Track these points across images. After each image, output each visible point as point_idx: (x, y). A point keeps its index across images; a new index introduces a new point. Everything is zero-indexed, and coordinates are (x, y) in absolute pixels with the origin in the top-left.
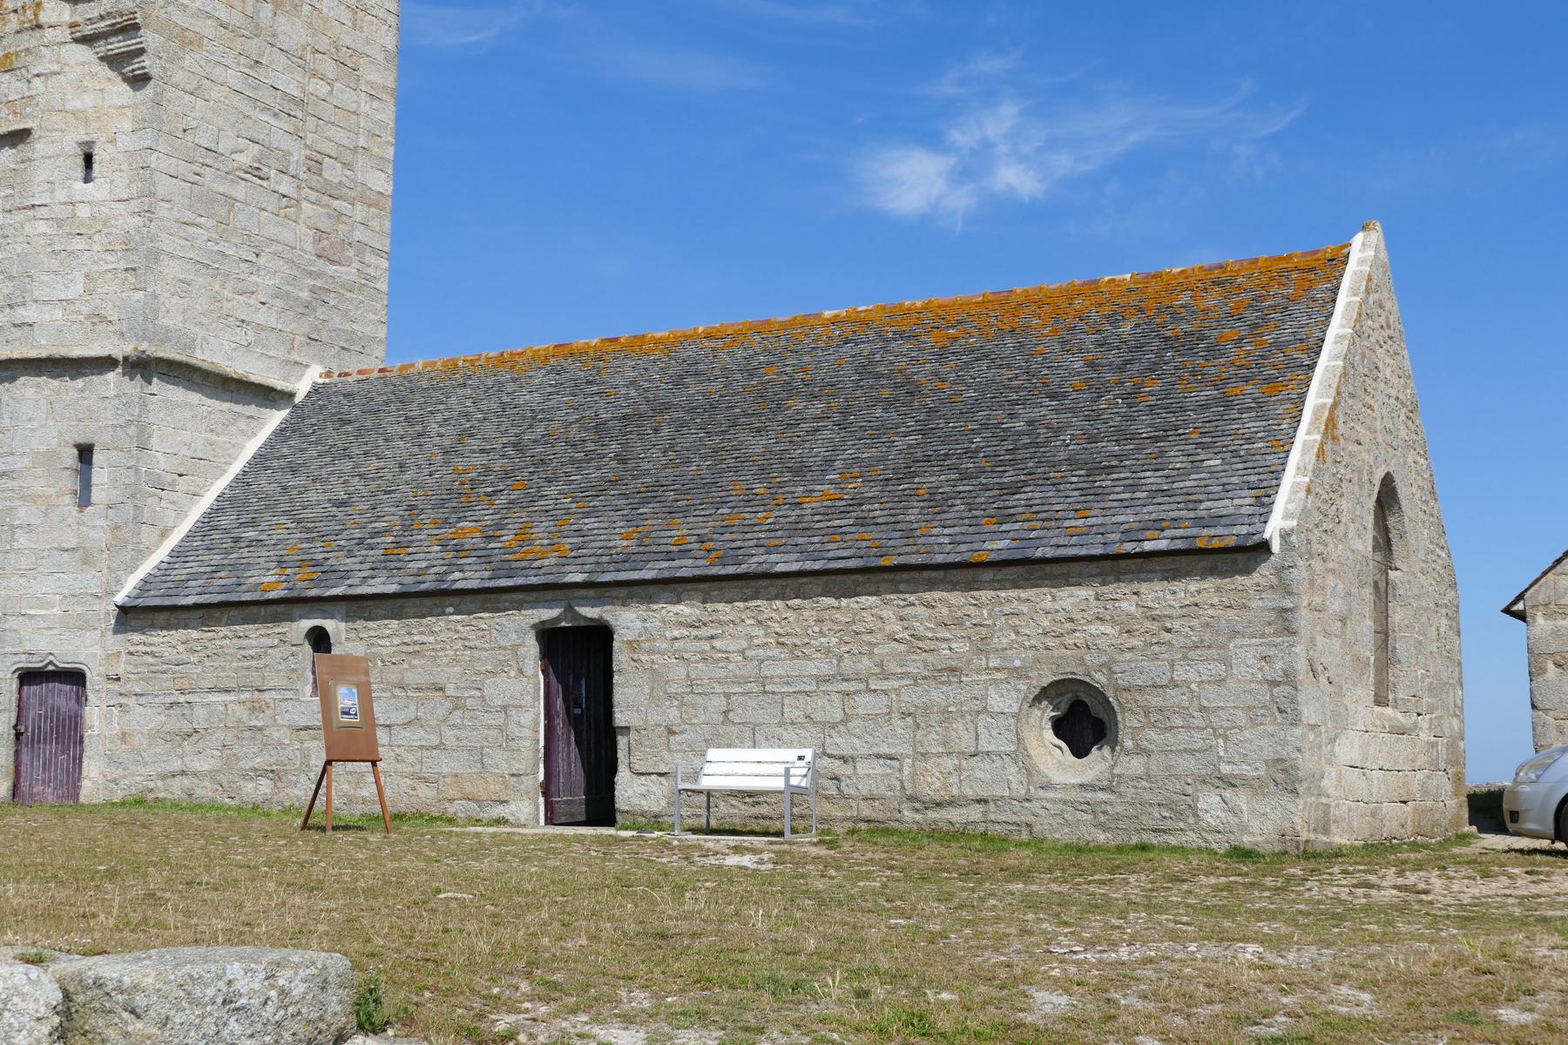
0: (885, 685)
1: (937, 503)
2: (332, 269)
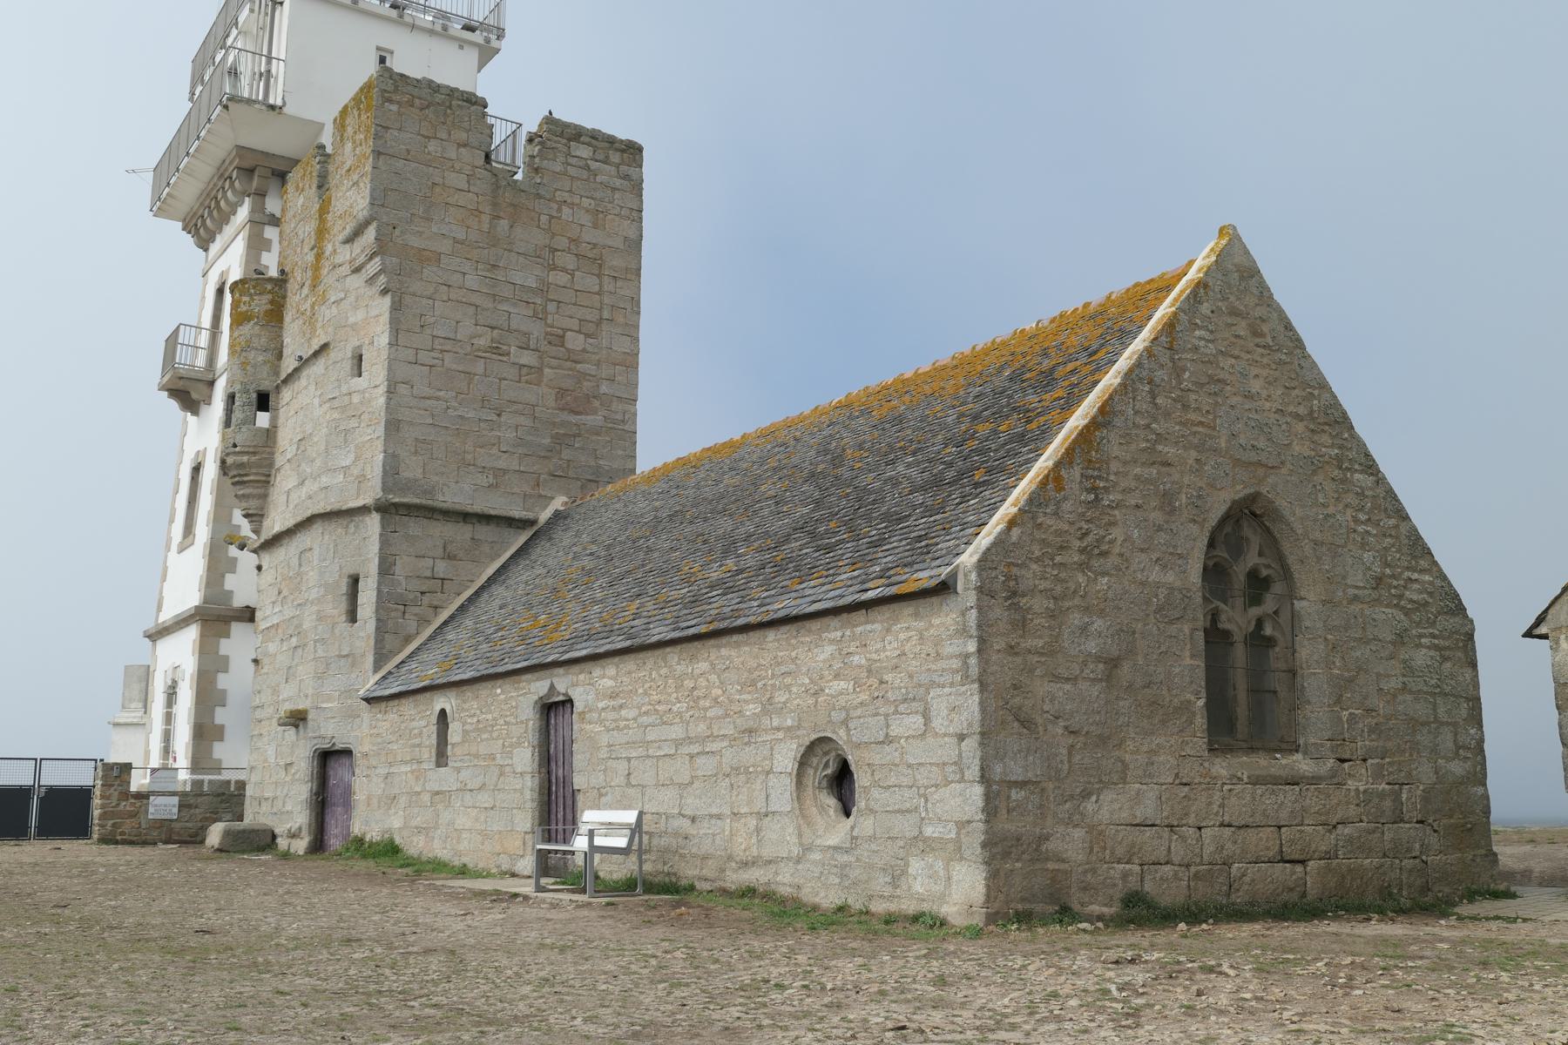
2: (573, 419)
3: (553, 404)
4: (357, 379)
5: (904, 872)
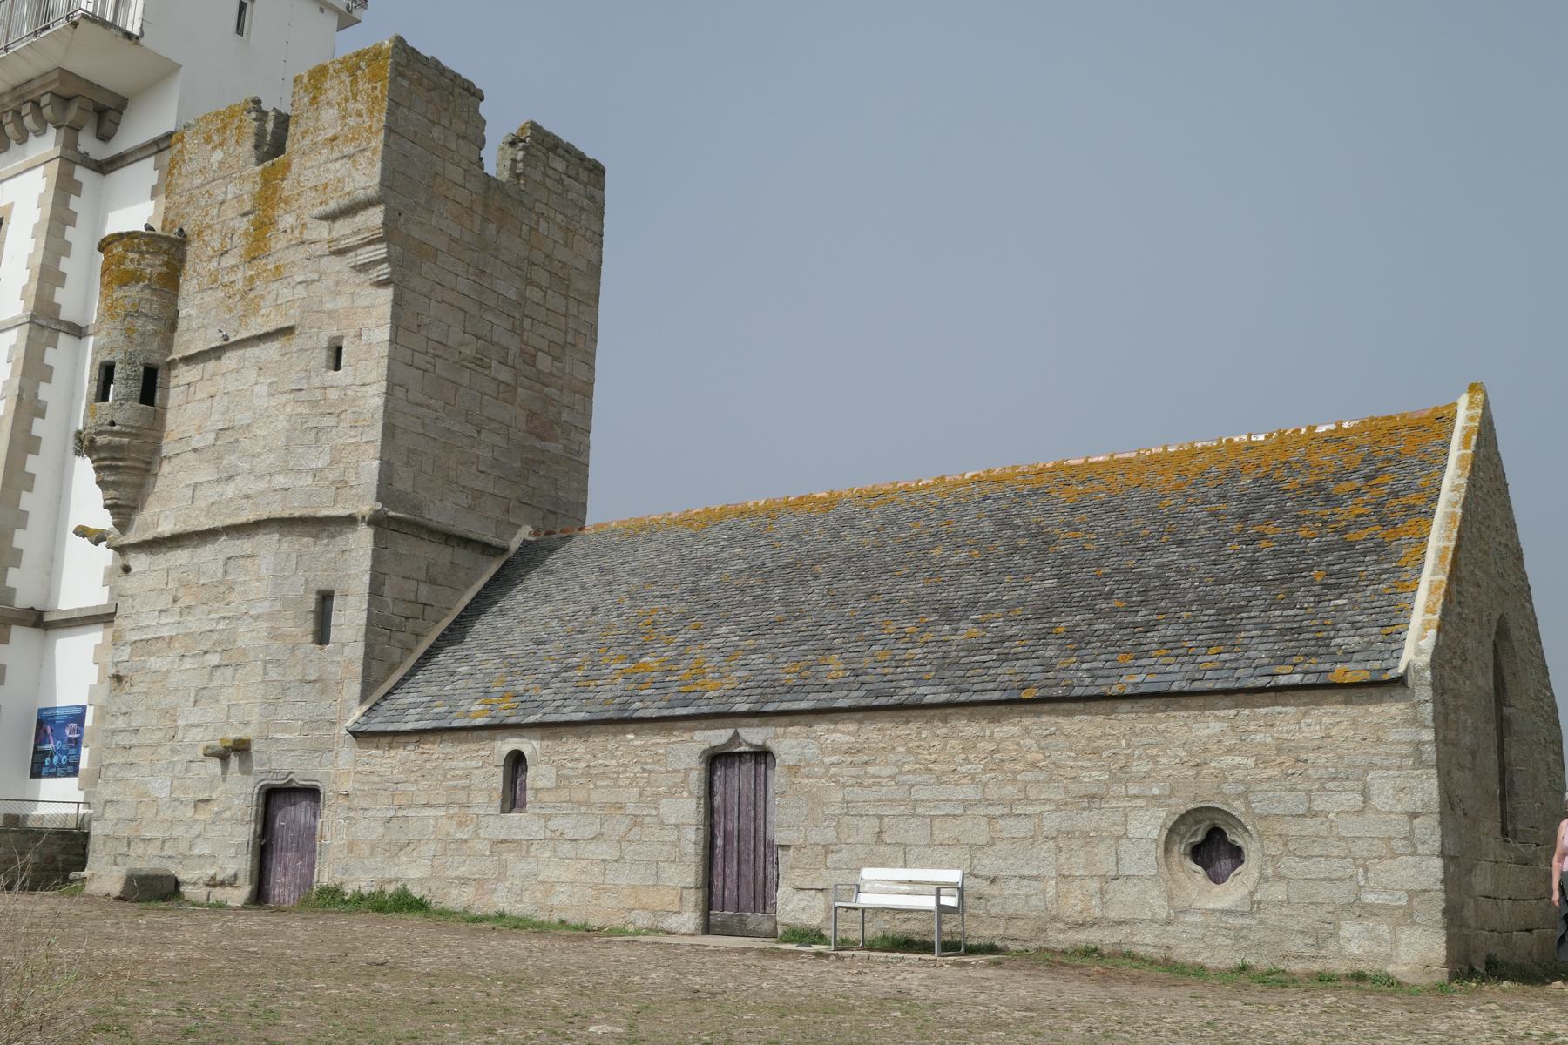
0: (1030, 810)
1: (1076, 641)
2: (539, 444)
3: (523, 427)
4: (332, 373)
5: (1333, 935)
